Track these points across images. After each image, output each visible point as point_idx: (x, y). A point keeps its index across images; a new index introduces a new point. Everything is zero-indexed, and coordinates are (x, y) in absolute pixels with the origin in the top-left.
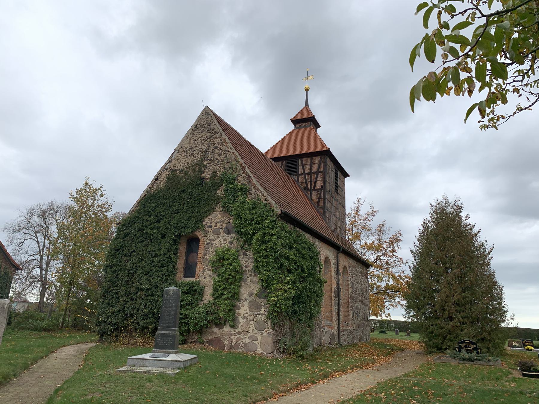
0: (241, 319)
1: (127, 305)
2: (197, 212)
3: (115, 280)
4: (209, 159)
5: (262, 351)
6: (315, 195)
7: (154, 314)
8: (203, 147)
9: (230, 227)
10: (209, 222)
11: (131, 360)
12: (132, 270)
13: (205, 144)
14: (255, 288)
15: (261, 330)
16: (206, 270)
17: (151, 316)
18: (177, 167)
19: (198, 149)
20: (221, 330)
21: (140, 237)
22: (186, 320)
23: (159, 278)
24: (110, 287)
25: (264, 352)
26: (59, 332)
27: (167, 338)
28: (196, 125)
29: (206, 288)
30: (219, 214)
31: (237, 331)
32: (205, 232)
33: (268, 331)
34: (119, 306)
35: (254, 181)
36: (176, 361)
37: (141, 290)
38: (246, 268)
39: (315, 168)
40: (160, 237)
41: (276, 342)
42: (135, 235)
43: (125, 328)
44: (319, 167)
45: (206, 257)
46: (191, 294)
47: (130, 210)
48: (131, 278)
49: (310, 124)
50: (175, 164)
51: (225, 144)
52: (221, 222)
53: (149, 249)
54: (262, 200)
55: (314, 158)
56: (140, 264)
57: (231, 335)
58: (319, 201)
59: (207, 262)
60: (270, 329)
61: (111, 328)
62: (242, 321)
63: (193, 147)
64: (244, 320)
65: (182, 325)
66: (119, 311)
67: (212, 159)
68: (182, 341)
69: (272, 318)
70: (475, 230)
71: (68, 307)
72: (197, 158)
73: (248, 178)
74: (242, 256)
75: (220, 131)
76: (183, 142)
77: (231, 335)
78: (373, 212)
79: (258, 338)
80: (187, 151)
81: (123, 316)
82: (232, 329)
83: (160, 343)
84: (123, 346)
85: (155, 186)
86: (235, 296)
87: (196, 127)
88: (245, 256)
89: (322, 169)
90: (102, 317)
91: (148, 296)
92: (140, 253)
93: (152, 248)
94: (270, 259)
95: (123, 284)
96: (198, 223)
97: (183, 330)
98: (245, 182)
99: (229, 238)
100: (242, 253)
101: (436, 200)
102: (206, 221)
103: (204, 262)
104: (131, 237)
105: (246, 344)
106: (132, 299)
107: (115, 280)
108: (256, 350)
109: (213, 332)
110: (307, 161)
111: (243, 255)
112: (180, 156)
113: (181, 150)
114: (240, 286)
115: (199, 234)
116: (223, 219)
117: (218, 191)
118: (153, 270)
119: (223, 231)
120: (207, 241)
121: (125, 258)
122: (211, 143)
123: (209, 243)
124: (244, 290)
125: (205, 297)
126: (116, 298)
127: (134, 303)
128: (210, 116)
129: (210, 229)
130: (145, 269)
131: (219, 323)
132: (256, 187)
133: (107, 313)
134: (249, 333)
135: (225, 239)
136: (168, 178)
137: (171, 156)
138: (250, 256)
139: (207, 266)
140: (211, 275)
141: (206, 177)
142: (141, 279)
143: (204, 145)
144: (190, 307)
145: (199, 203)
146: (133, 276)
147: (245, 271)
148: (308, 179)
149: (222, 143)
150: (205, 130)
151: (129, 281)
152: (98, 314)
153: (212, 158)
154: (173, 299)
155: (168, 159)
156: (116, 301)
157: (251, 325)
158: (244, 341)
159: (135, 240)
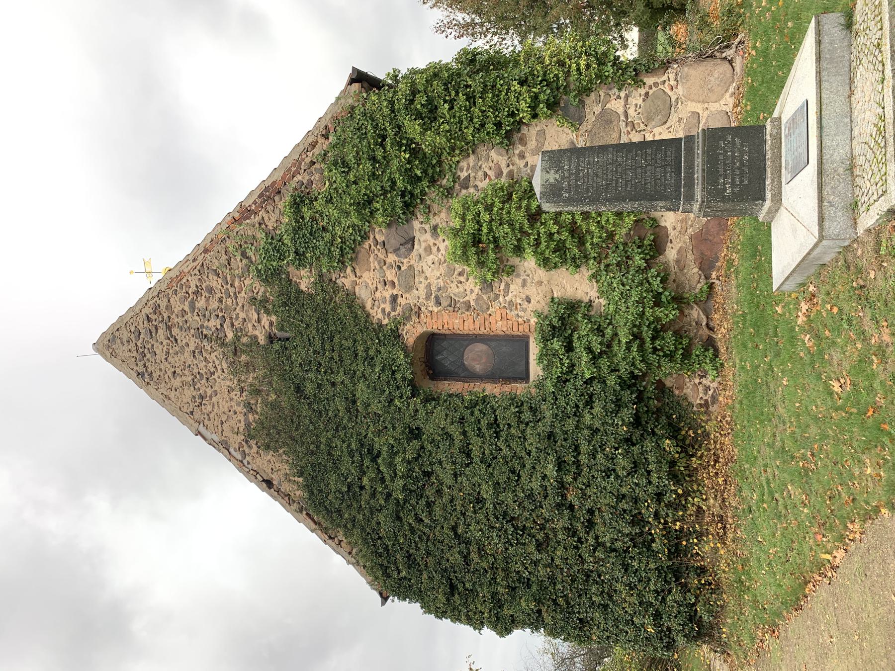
2: (355, 341)
3: (534, 588)
4: (221, 325)
5: (728, 95)
9: (394, 242)
10: (382, 306)
11: (827, 224)
12: (506, 531)
13: (184, 342)
15: (668, 105)
16: (508, 298)
17: (636, 449)
18: (240, 421)
19: (195, 362)
20: (672, 234)
22: (647, 334)
24: (554, 601)
25: (731, 90)
27: (721, 157)
28: (138, 374)
29: (555, 296)
30: (360, 277)
33: (673, 83)
34: (610, 568)
37: (564, 496)
38: (502, 173)
40: (416, 444)
45: (472, 303)
47: (349, 562)
51: (184, 280)
52: (381, 267)
54: (325, 147)
59: (485, 297)
60: (665, 78)
61: (676, 594)
63: (190, 379)
66: (626, 567)
67: (221, 315)
68: (707, 350)
72: (217, 362)
73: (269, 197)
74: (471, 190)
75: (153, 298)
76: (177, 411)
79: (692, 112)
83: (742, 181)
88: (471, 183)
91: (577, 463)
99: (423, 239)
100: (464, 192)
102: (380, 316)
103: (485, 306)
104: (416, 546)
109: (677, 261)
112: (212, 416)
115: (411, 333)
116: (374, 264)
117: (303, 287)
118: (504, 458)
119: (405, 261)
120: (432, 303)
121: (474, 556)
122: (181, 324)
123: (437, 298)
126: (587, 581)
128: (117, 334)
129: (400, 300)
130: (502, 479)
132: (293, 169)
135: (425, 249)
136: (268, 447)
137: (212, 443)
138: (471, 165)
139: (497, 297)
140: (519, 281)
141: (266, 327)
143: (188, 345)
145: (331, 338)
147: (511, 175)
149: (181, 288)
150: (150, 346)
151: (537, 540)
153: (217, 316)
154: (578, 165)
155: (219, 451)
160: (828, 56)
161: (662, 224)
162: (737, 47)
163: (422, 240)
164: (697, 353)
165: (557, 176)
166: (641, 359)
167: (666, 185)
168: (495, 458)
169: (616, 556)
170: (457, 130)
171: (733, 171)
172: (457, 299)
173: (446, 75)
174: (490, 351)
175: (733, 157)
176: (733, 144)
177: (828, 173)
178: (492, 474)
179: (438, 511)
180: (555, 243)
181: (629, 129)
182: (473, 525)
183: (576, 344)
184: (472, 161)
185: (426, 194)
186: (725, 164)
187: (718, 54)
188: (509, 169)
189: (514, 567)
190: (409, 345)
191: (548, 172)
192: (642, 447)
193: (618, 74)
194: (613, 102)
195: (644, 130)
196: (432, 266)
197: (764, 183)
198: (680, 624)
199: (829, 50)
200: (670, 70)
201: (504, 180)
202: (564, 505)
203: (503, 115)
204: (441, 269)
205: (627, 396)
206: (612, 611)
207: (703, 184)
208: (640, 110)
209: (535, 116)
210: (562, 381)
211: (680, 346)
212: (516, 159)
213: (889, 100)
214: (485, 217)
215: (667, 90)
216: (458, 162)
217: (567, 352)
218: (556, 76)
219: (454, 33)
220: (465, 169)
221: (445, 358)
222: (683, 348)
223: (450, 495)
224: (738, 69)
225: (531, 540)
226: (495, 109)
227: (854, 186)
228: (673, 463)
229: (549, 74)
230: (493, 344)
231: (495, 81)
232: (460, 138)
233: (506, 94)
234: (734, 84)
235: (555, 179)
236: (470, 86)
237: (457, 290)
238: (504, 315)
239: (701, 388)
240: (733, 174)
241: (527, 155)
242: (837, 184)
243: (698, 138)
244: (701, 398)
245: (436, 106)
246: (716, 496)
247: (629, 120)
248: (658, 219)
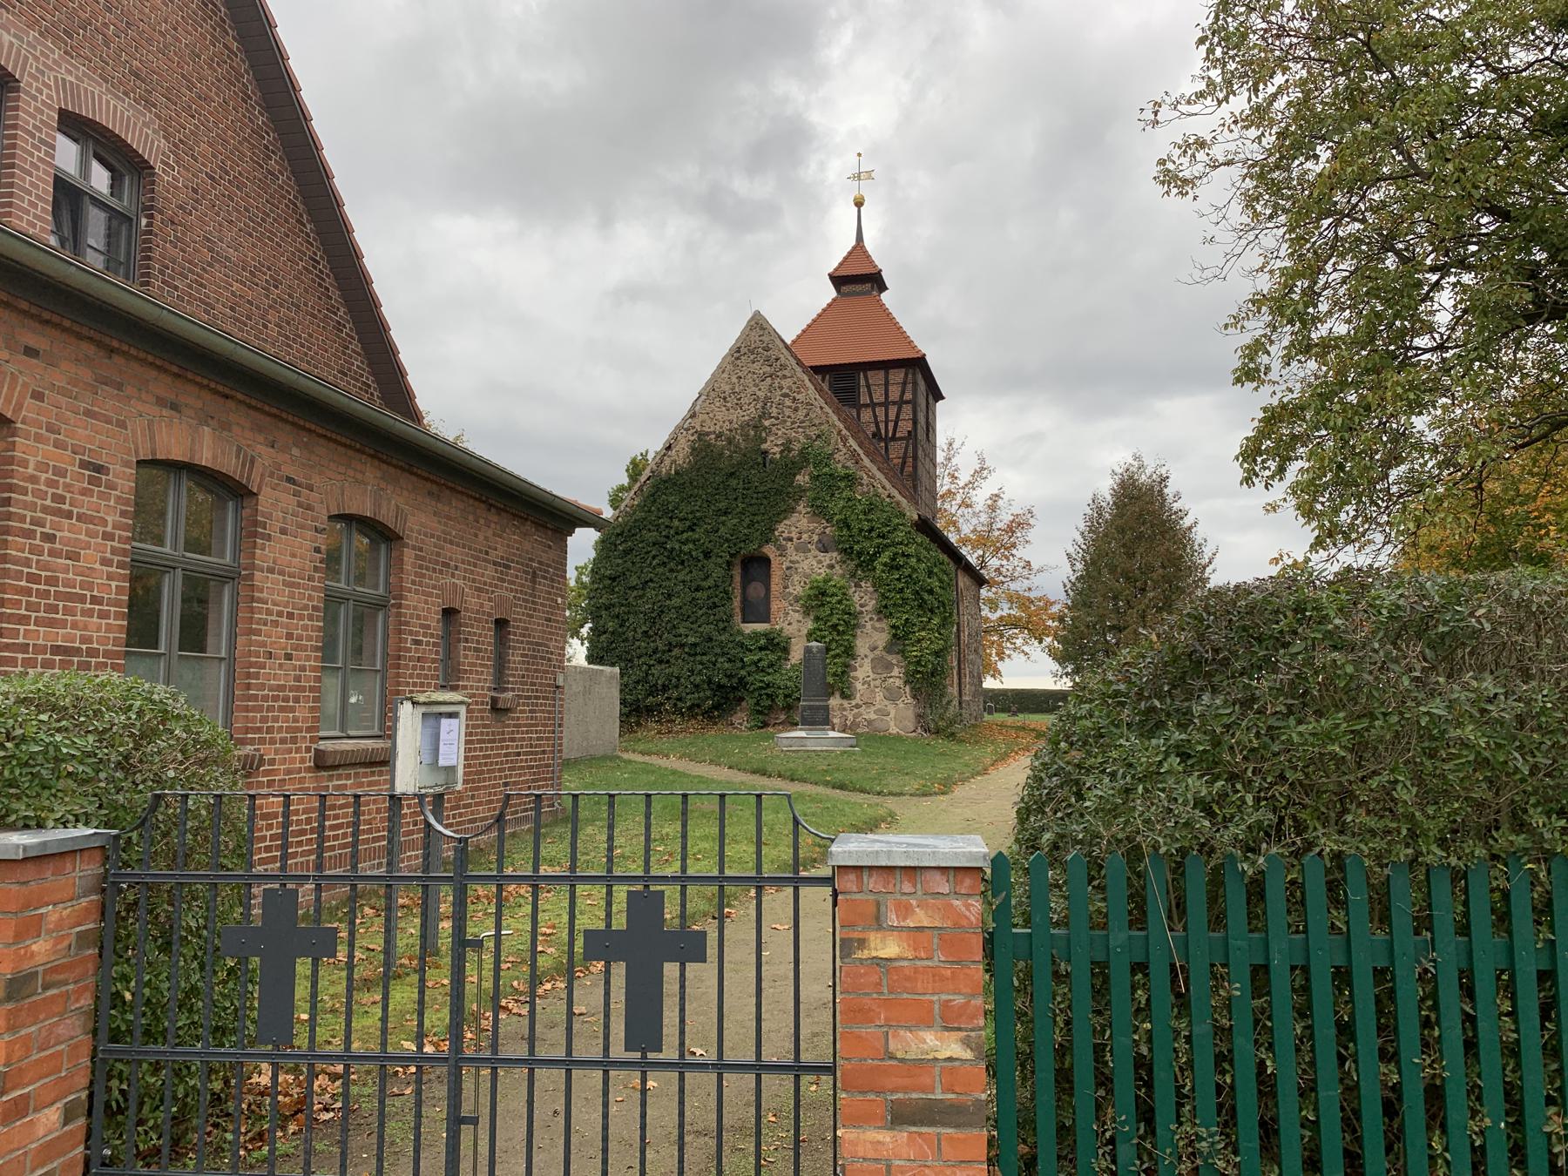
0: (859, 686)
6: (896, 450)
8: (759, 393)
14: (882, 639)
17: (706, 686)
22: (769, 691)
31: (854, 703)
32: (782, 551)
35: (866, 462)
39: (894, 393)
41: (919, 716)
44: (903, 393)
49: (872, 288)
50: (703, 421)
53: (680, 577)
55: (891, 371)
57: (845, 709)
58: (904, 463)
66: (638, 682)
70: (1187, 522)
76: (714, 378)
77: (845, 709)
78: (983, 469)
80: (725, 398)
85: (667, 461)
86: (849, 652)
87: (738, 352)
89: (908, 396)
91: (696, 654)
94: (908, 593)
96: (768, 537)
98: (849, 464)
99: (827, 558)
101: (1122, 463)
105: (870, 722)
106: (660, 662)
110: (876, 377)
113: (712, 393)
114: (854, 636)
115: (770, 550)
116: (812, 526)
117: (798, 477)
125: (792, 654)
137: (694, 404)
144: (771, 670)
147: (862, 613)
148: (882, 417)
179: (661, 570)
201: (858, 608)
205: (735, 681)
210: (742, 645)
226: (894, 605)
228: (698, 706)
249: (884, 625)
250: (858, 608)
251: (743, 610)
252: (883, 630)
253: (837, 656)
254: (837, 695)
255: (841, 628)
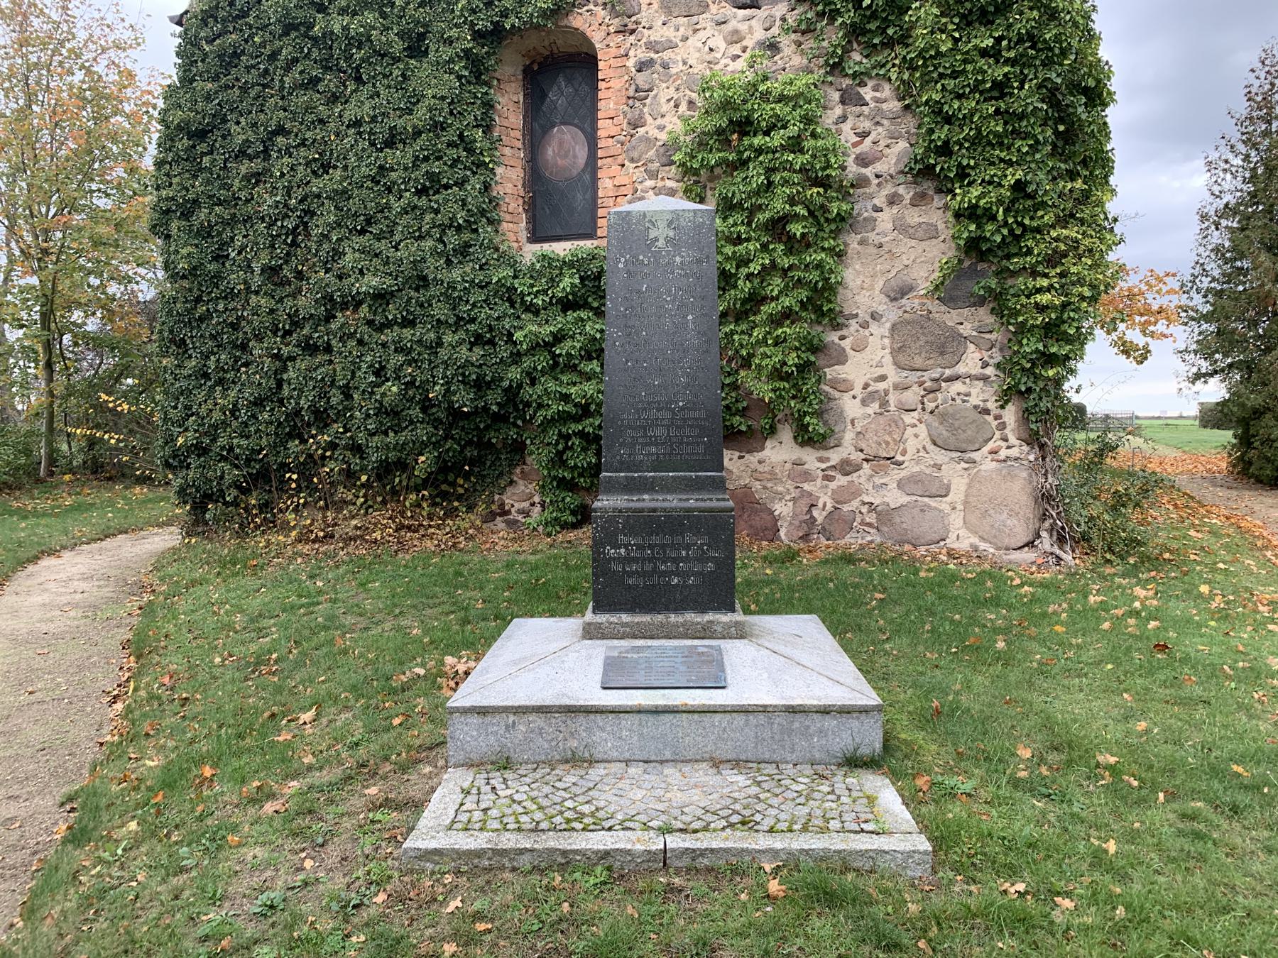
0: (851, 407)
1: (292, 374)
3: (213, 267)
7: (426, 405)
11: (475, 720)
12: (286, 216)
15: (964, 446)
17: (416, 412)
20: (752, 459)
21: (296, 60)
22: (588, 425)
23: (428, 244)
24: (198, 300)
25: (983, 546)
26: (36, 492)
27: (678, 539)
31: (835, 457)
33: (1003, 454)
34: (253, 381)
36: (825, 711)
37: (344, 306)
40: (398, 47)
42: (273, 56)
43: (309, 466)
45: (641, 131)
46: (592, 308)
48: (288, 254)
53: (350, 113)
56: (316, 185)
57: (808, 476)
59: (651, 153)
60: (1013, 440)
62: (858, 415)
64: (870, 410)
65: (571, 448)
66: (259, 403)
68: (573, 513)
69: (1029, 390)
71: (55, 407)
74: (838, 111)
77: (808, 476)
81: (280, 424)
82: (808, 450)
83: (631, 574)
84: (305, 548)
88: (851, 109)
90: (186, 430)
91: (388, 325)
92: (308, 135)
93: (368, 104)
95: (256, 281)
97: (576, 466)
100: (836, 96)
103: (635, 155)
104: (253, 67)
105: (885, 516)
106: (310, 348)
107: (213, 267)
108: (942, 533)
111: (843, 102)
114: (840, 255)
120: (641, 54)
124: (858, 273)
126: (236, 347)
127: (321, 365)
130: (353, 205)
131: (743, 428)
133: (203, 411)
134: (899, 464)
135: (736, 32)
138: (884, 106)
139: (653, 175)
142: (337, 254)
146: (294, 244)
147: (861, 182)
152: (165, 420)
156: (236, 360)
157: (910, 431)
158: (876, 502)
159: (277, 78)
160: (796, 725)
161: (769, 444)
162: (1052, 554)
163: (753, 22)
164: (568, 499)
165: (661, 243)
166: (549, 417)
167: (633, 446)
168: (389, 190)
169: (270, 389)
170: (941, 70)
171: (650, 560)
172: (648, 101)
173: (1047, 36)
174: (575, 172)
175: (676, 560)
176: (702, 559)
177: (569, 722)
178: (362, 186)
179: (303, 98)
180: (733, 271)
181: (928, 384)
182: (289, 160)
183: (571, 315)
184: (891, 106)
185: (832, 20)
186: (663, 546)
187: (1047, 524)
188: (872, 177)
189: (240, 231)
190: (571, 18)
191: (670, 223)
192: (421, 423)
193: (1024, 362)
194: (977, 355)
195: (923, 409)
196: (707, 49)
197: (627, 611)
198: (194, 481)
199: (808, 727)
200: (1026, 448)
201: (853, 169)
202: (331, 305)
203: (963, 156)
204: (701, 67)
205: (493, 399)
206: (201, 385)
207: (628, 510)
208: (959, 401)
209: (958, 215)
210: (511, 296)
211: (576, 475)
212: (888, 189)
213: (629, 840)
214: (776, 139)
215: (991, 445)
216: (890, 80)
217: (560, 301)
218: (1029, 252)
219: (1257, 83)
220: (878, 95)
221: (560, 94)
222: (573, 478)
223: (329, 117)
224: (1016, 556)
225: (280, 258)
226: (977, 141)
227: (538, 765)
228: (402, 465)
229: (1034, 238)
230: (587, 177)
231: (1027, 136)
232: (927, 78)
233: (1002, 160)
234: (992, 550)
235: (656, 239)
236: (1021, 88)
237: (663, 100)
238: (623, 191)
239: (526, 504)
240: (644, 559)
241: (895, 209)
242: (547, 738)
243: (718, 500)
244: (513, 506)
245: (992, 22)
246: (360, 528)
247: (943, 384)
248: (776, 437)
249: (935, 215)
250: (853, 169)
251: (532, 208)
252: (931, 233)
253: (787, 316)
254: (786, 433)
255: (797, 229)
